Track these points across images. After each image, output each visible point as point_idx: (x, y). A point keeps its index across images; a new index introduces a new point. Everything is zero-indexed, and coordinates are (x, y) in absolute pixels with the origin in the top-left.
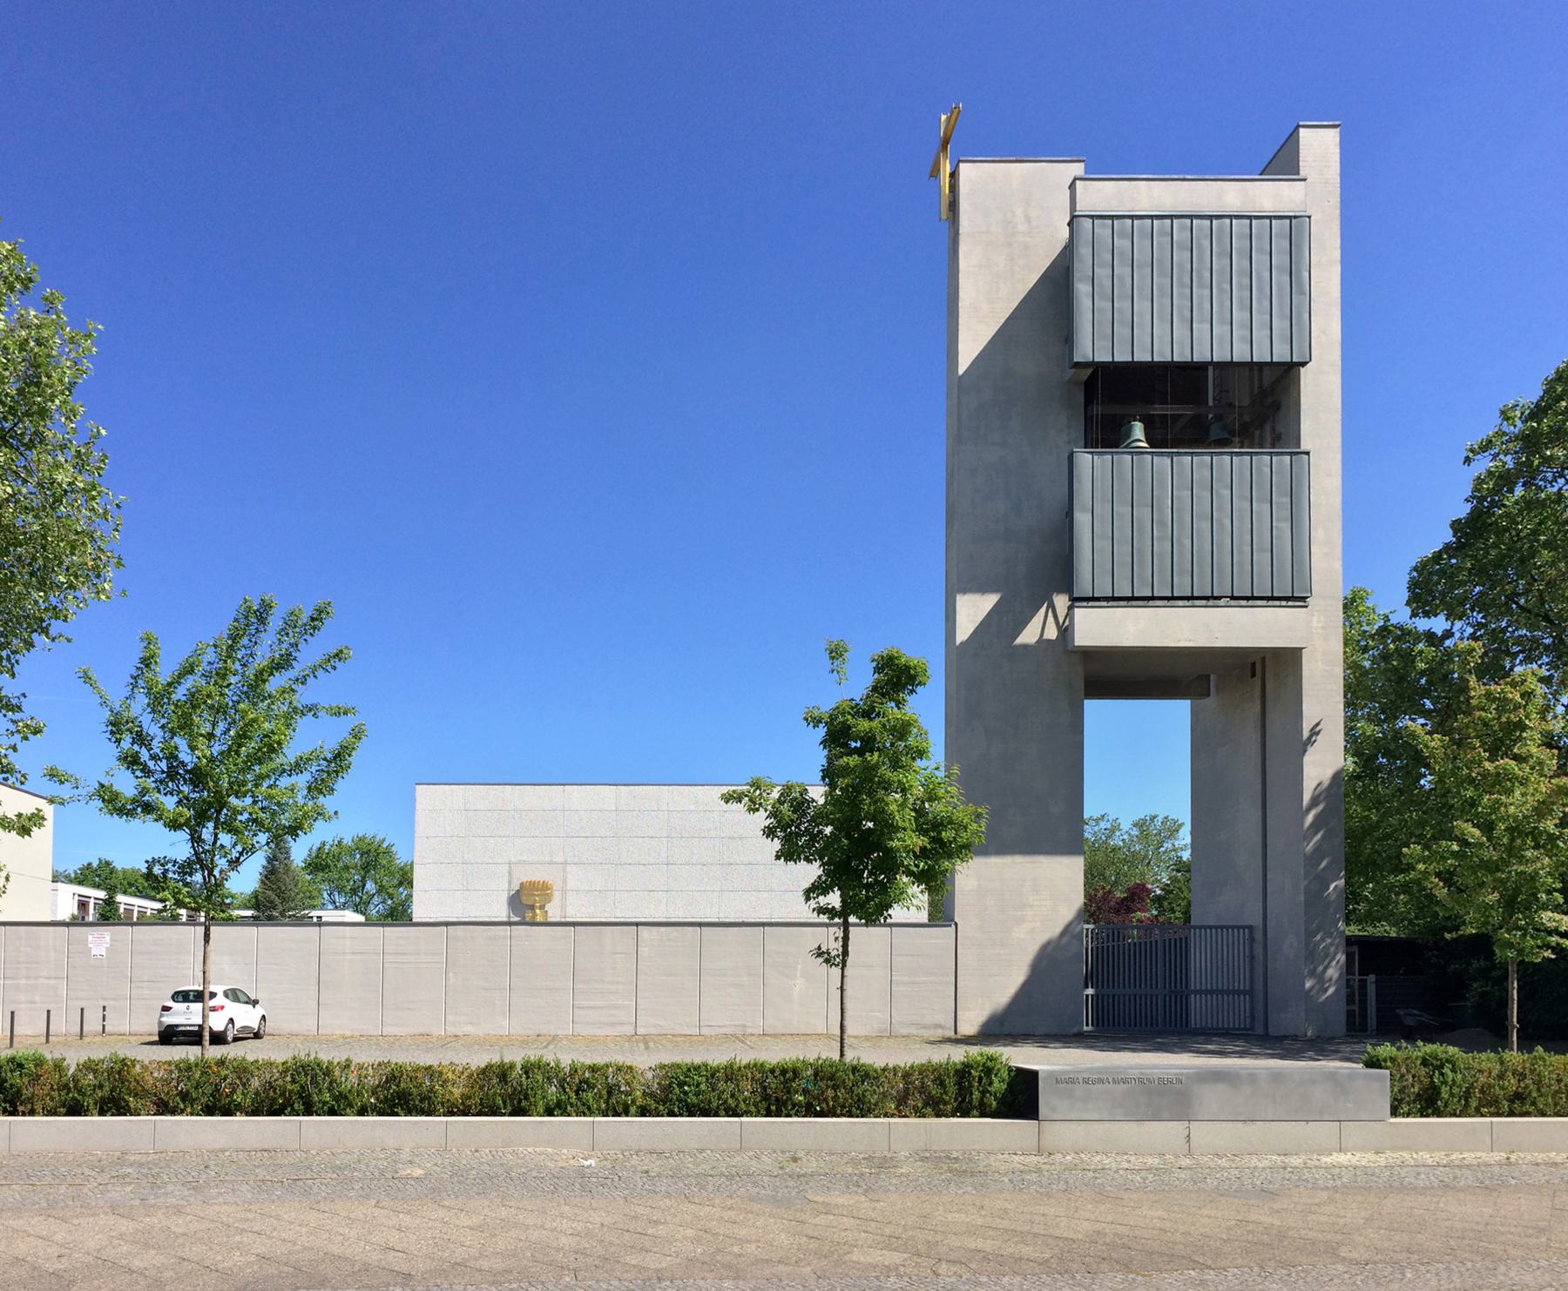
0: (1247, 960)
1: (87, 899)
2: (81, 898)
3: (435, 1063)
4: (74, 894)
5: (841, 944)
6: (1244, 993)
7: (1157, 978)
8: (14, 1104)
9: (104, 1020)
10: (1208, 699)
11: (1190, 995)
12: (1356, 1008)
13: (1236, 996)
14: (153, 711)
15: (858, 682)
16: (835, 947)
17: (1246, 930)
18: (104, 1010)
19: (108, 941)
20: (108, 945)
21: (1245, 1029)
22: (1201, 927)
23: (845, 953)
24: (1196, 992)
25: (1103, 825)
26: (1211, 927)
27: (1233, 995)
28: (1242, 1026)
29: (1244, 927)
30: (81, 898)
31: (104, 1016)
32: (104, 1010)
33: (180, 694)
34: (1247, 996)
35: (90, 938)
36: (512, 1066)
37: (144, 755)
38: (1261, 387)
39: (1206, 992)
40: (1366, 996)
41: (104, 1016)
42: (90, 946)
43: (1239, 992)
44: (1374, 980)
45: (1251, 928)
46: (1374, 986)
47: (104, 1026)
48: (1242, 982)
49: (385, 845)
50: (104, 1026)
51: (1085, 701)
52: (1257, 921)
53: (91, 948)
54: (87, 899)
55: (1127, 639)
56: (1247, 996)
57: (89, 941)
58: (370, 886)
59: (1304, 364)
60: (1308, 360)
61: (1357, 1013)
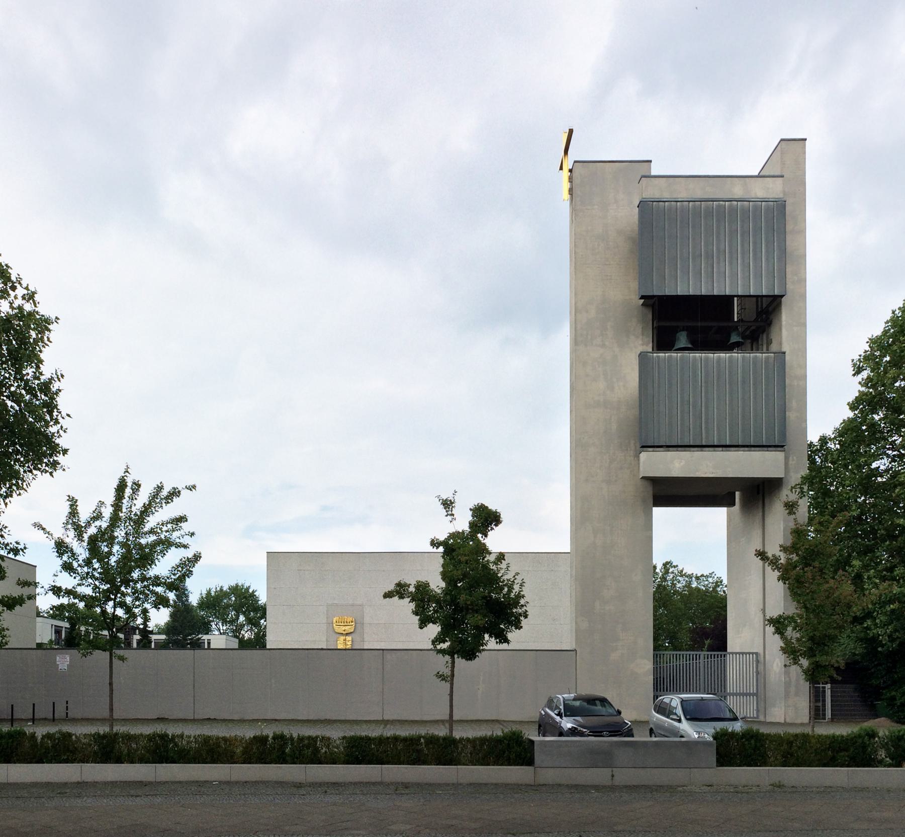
0: (755, 674)
1: (60, 629)
2: (56, 628)
3: (228, 736)
4: (52, 625)
5: (450, 669)
6: (753, 695)
7: (700, 686)
8: (8, 758)
9: (67, 710)
10: (735, 507)
11: (727, 696)
12: (820, 704)
13: (751, 697)
14: (79, 539)
15: (462, 522)
16: (447, 671)
17: (754, 655)
18: (67, 703)
19: (68, 660)
20: (68, 663)
21: (754, 718)
22: (733, 653)
23: (453, 675)
24: (730, 694)
25: (710, 580)
26: (736, 653)
27: (746, 696)
28: (752, 716)
29: (753, 653)
30: (56, 628)
31: (67, 707)
32: (67, 703)
33: (92, 530)
34: (755, 697)
35: (58, 658)
36: (267, 737)
37: (75, 564)
38: (762, 308)
39: (736, 694)
40: (825, 697)
41: (67, 707)
42: (58, 663)
43: (750, 694)
44: (830, 687)
45: (757, 654)
46: (829, 690)
47: (67, 713)
48: (751, 688)
49: (251, 591)
50: (67, 713)
51: (655, 509)
52: (761, 651)
53: (58, 665)
54: (60, 629)
55: (675, 472)
56: (755, 697)
57: (57, 660)
58: (242, 618)
59: (782, 296)
60: (784, 294)
61: (821, 708)
